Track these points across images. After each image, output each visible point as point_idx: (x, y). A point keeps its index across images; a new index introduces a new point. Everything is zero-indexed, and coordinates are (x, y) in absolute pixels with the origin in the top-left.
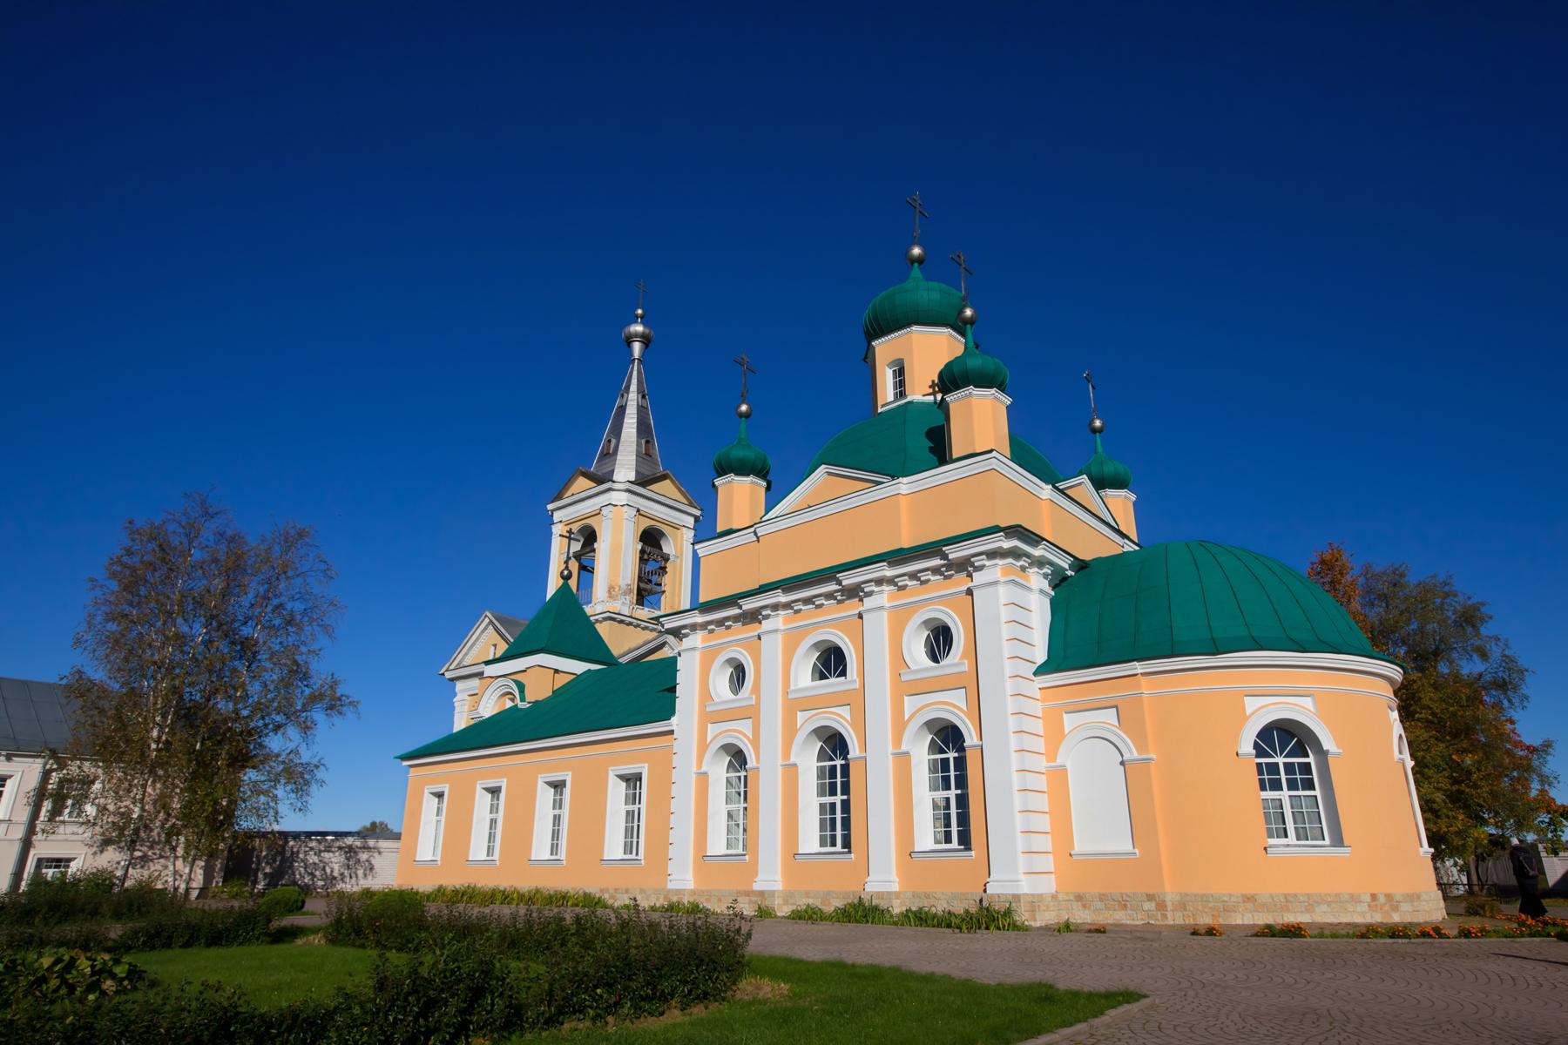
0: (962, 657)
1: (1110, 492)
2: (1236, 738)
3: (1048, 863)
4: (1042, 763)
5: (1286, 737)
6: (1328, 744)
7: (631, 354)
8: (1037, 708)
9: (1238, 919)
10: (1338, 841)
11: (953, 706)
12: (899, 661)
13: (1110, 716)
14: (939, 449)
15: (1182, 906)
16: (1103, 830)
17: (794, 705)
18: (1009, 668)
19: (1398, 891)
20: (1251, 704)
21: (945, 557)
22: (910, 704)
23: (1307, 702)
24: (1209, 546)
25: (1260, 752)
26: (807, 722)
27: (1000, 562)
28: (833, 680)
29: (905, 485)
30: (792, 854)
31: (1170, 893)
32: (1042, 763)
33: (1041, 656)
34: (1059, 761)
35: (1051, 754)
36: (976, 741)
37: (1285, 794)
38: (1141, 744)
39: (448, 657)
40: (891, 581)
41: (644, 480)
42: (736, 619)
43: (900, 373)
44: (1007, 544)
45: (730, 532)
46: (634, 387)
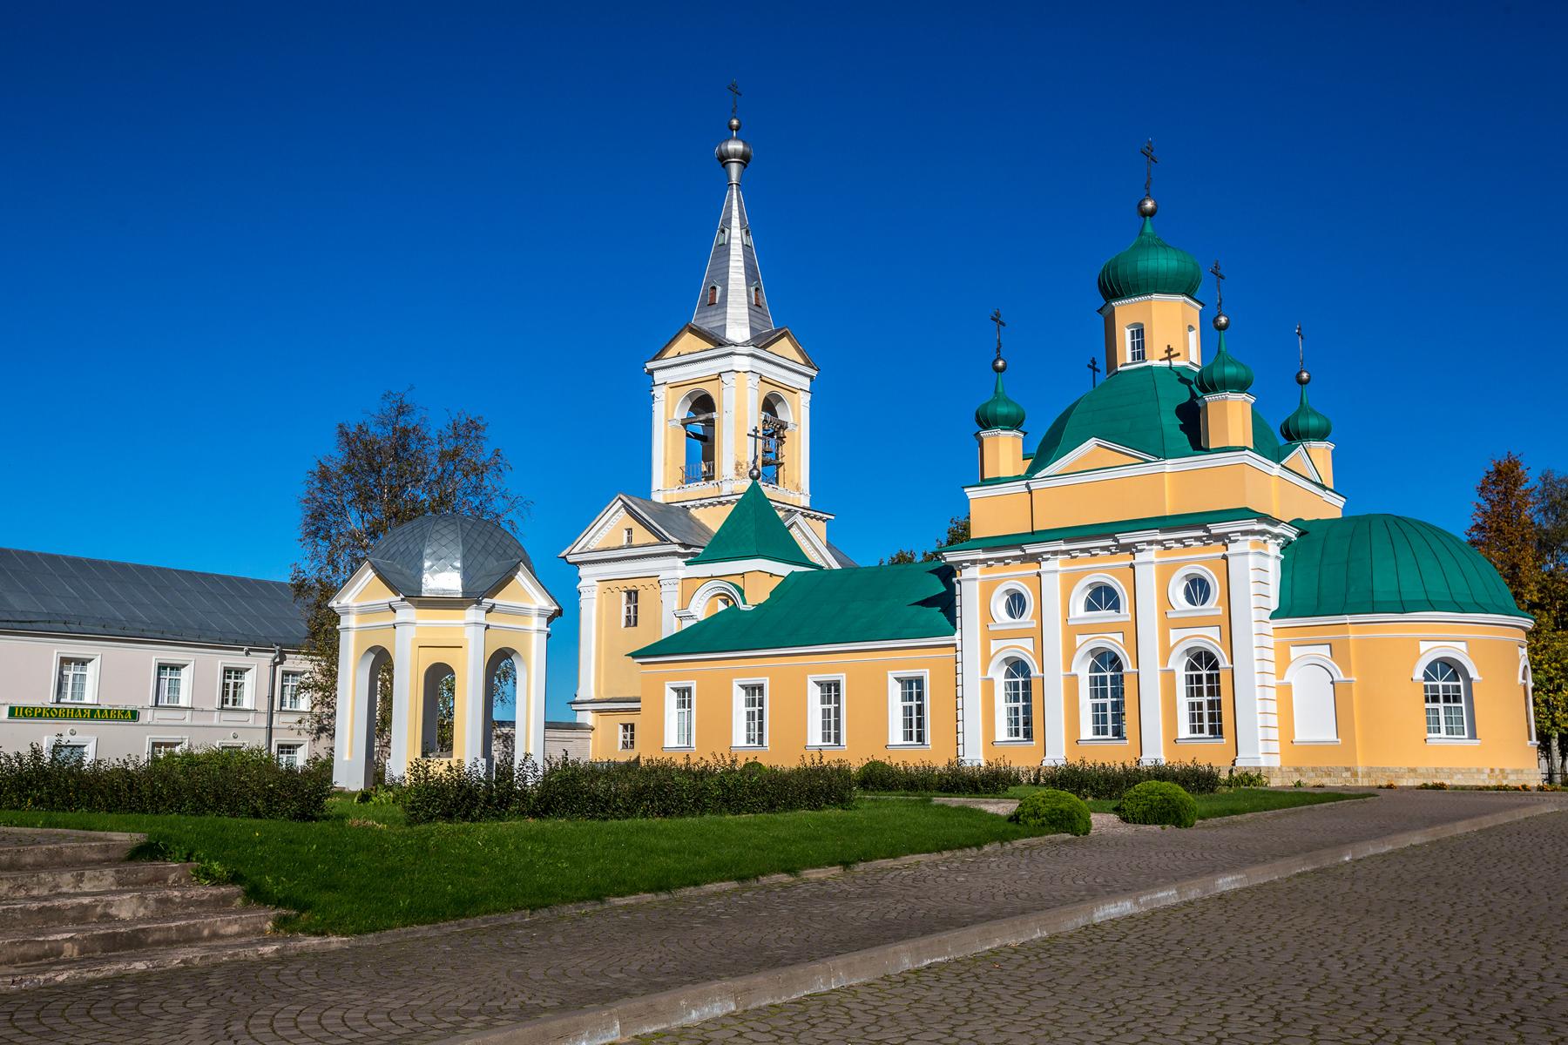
0: (1219, 604)
1: (1314, 444)
2: (1412, 669)
3: (1275, 747)
4: (1272, 680)
5: (1448, 667)
6: (1473, 674)
7: (729, 178)
8: (1270, 642)
9: (1404, 783)
10: (1473, 736)
11: (1209, 638)
12: (1165, 602)
13: (1325, 650)
14: (1194, 430)
15: (1368, 774)
16: (1315, 724)
17: (1071, 631)
18: (1254, 615)
19: (1508, 767)
20: (1424, 646)
21: (1208, 531)
22: (1175, 635)
23: (1462, 646)
24: (1402, 523)
25: (1427, 678)
26: (1085, 643)
27: (1250, 538)
28: (1104, 612)
29: (1169, 465)
30: (991, 742)
31: (1361, 766)
32: (1272, 680)
33: (1274, 604)
34: (1286, 679)
35: (1280, 674)
36: (1228, 664)
37: (1441, 706)
38: (1347, 672)
39: (571, 539)
40: (1160, 543)
41: (761, 340)
42: (1015, 558)
43: (1139, 333)
44: (1258, 527)
45: (997, 481)
46: (735, 222)
